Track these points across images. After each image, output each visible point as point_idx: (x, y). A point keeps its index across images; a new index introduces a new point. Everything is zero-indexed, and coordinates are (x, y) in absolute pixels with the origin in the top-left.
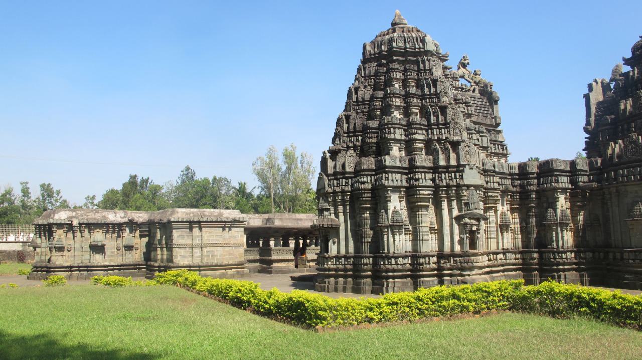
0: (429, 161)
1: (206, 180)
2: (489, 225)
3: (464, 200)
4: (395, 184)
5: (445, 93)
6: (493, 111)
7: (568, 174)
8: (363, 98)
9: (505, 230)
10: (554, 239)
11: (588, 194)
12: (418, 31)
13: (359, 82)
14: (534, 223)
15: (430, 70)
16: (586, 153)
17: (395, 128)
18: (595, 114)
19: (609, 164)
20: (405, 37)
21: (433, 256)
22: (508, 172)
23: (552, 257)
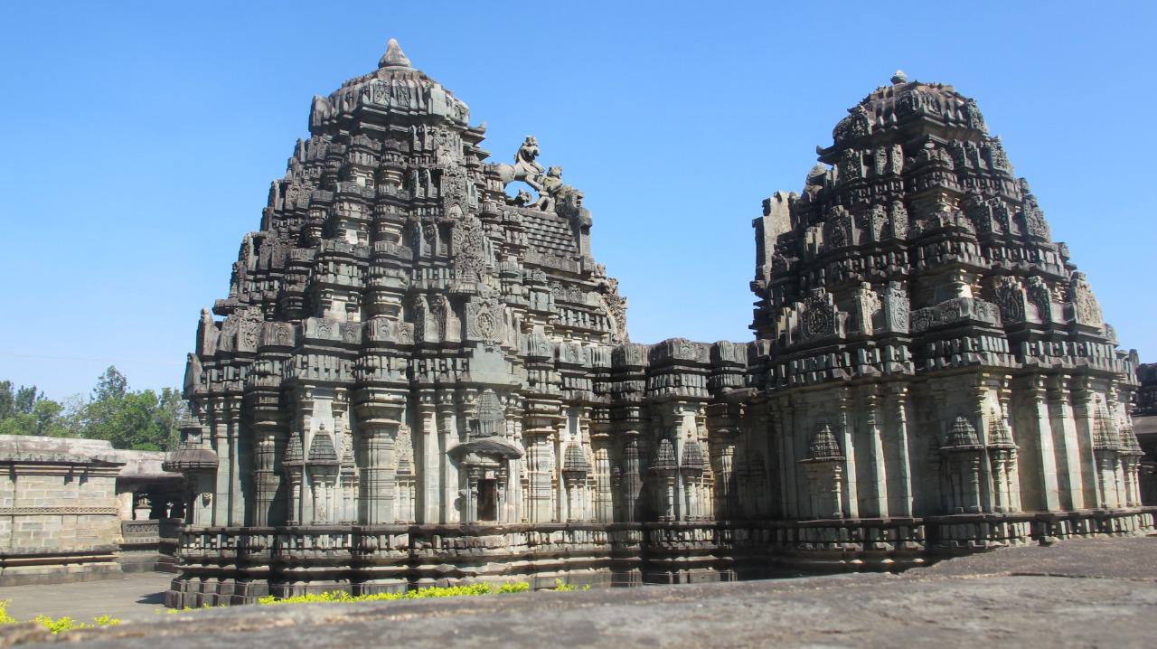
0: (404, 332)
1: (149, 395)
2: (535, 471)
3: (470, 414)
4: (323, 377)
5: (455, 198)
6: (578, 246)
7: (703, 370)
8: (294, 204)
9: (575, 483)
10: (671, 501)
11: (742, 412)
12: (424, 78)
13: (293, 173)
14: (637, 470)
15: (432, 152)
16: (754, 333)
17: (337, 263)
18: (773, 258)
19: (780, 349)
20: (392, 88)
21: (397, 534)
22: (589, 365)
23: (665, 538)
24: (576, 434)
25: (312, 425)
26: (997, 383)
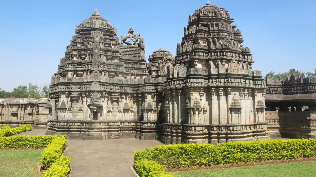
4: (62, 90)
17: (69, 65)
24: (127, 100)
25: (61, 100)
26: (199, 90)
